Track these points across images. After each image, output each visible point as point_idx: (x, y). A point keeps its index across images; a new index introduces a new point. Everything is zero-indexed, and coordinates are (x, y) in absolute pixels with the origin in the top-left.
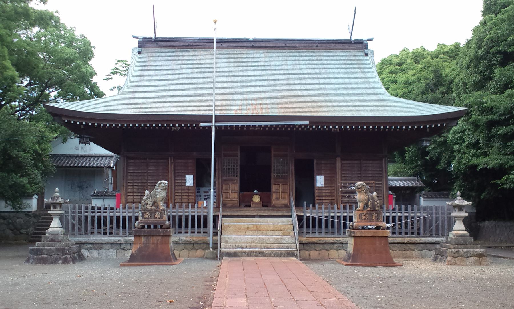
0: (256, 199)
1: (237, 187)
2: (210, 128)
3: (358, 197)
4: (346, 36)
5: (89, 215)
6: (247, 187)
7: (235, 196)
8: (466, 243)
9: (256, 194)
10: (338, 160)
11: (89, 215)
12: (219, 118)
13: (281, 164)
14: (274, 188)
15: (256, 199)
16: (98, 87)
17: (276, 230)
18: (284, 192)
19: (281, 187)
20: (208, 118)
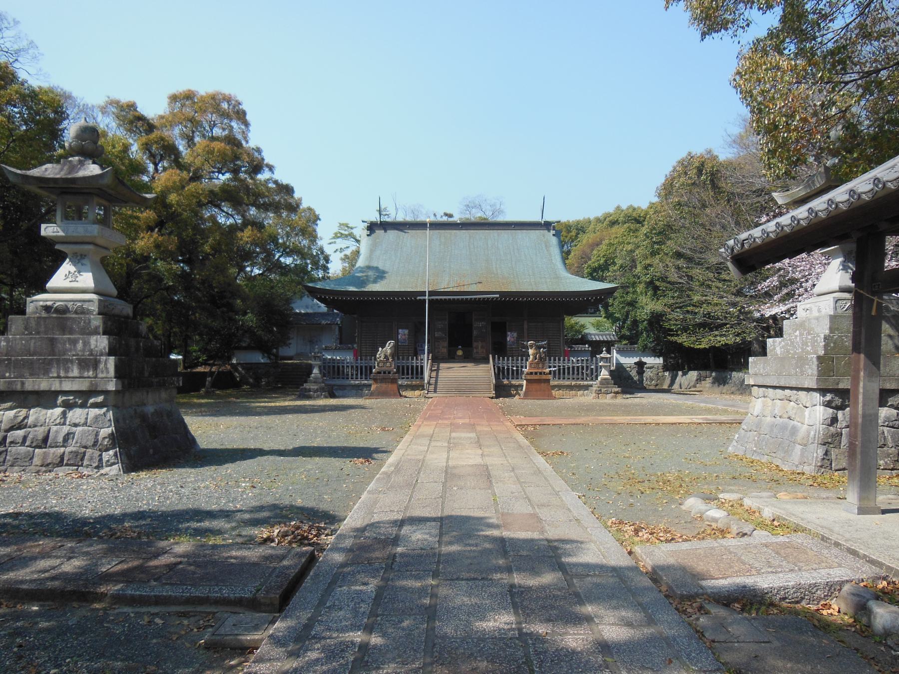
0: (460, 353)
1: (446, 344)
2: (425, 300)
3: (531, 351)
4: (536, 218)
5: (364, 365)
6: (453, 344)
7: (445, 350)
8: (608, 384)
9: (278, 352)
10: (526, 322)
11: (364, 365)
12: (431, 293)
13: (479, 326)
14: (475, 344)
15: (460, 353)
16: (668, 189)
17: (482, 373)
18: (482, 347)
19: (480, 344)
20: (423, 293)
